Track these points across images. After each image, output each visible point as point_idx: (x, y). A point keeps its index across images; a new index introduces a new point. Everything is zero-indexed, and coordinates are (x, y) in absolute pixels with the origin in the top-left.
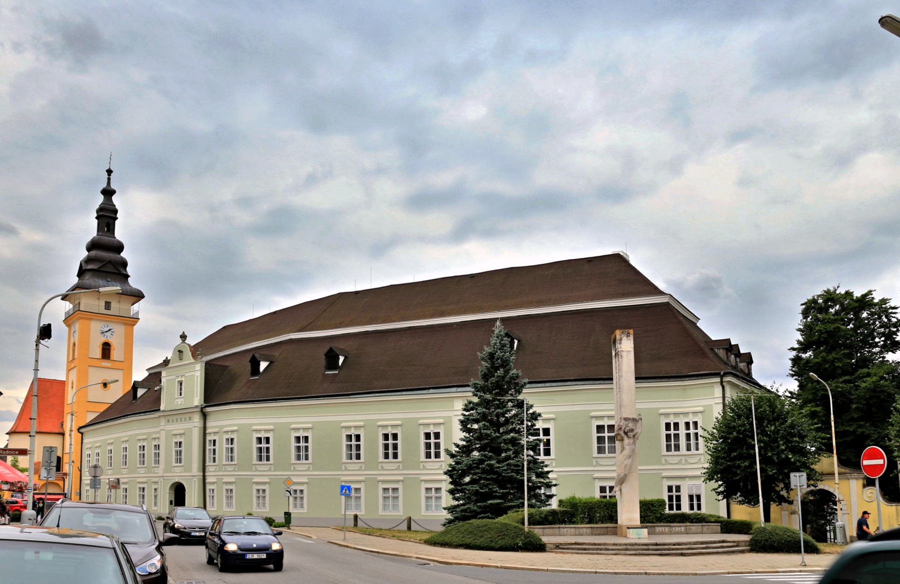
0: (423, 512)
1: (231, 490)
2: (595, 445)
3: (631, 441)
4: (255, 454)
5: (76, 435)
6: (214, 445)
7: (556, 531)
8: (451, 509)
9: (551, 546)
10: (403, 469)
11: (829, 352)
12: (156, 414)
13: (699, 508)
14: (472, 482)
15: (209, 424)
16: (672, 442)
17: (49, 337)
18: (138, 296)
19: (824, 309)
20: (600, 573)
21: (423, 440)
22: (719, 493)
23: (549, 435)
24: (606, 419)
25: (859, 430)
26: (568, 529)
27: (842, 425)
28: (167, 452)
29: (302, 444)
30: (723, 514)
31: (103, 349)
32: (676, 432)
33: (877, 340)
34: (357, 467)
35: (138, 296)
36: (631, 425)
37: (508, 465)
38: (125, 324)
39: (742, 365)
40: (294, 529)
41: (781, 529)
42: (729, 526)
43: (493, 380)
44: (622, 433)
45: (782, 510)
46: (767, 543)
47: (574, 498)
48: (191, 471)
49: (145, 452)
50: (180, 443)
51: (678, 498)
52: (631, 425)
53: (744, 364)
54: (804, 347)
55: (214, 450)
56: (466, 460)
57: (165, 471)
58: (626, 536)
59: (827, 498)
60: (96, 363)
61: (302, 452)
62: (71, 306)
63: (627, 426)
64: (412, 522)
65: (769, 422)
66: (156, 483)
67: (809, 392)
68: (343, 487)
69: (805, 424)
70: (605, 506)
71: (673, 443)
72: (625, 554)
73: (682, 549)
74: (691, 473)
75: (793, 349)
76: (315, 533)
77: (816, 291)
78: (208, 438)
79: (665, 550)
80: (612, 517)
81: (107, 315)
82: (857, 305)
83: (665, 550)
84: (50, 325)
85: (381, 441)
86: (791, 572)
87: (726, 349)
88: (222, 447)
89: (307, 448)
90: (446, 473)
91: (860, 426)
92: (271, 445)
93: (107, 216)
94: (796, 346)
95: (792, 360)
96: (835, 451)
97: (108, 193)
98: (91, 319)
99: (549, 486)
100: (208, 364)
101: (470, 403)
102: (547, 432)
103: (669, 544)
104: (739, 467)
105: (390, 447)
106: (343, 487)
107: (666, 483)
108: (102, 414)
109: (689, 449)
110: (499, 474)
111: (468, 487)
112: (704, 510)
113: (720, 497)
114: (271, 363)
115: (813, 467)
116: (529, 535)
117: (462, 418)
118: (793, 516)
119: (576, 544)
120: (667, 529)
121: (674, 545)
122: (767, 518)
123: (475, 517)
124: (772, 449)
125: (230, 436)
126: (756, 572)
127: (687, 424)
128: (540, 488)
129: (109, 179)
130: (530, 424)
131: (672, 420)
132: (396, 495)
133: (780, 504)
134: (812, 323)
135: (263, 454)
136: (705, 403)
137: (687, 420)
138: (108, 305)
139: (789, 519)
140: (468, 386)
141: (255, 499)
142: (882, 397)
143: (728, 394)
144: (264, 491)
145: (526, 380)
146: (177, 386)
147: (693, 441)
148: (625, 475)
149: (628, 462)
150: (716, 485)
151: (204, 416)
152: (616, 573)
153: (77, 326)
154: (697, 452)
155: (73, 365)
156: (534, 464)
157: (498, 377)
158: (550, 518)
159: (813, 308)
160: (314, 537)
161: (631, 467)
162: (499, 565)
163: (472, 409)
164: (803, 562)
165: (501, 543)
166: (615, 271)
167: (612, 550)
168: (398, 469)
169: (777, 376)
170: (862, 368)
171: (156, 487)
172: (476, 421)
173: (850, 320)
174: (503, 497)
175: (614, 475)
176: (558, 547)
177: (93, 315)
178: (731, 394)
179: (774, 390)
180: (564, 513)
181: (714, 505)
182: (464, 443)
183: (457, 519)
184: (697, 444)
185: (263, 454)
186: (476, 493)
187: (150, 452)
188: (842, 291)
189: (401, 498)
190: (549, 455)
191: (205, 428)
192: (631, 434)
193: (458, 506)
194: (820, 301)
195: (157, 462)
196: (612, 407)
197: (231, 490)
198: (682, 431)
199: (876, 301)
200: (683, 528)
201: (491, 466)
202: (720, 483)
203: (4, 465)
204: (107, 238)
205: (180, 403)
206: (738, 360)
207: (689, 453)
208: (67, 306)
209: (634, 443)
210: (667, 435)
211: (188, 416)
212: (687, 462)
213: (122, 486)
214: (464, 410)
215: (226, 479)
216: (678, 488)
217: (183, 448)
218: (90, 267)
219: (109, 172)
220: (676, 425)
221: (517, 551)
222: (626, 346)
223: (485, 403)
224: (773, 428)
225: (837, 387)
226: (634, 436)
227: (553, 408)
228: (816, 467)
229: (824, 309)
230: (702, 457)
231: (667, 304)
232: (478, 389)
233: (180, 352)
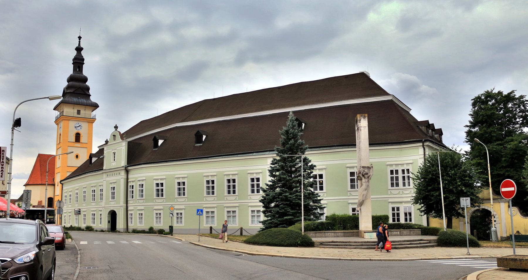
0: (250, 224)
1: (142, 214)
2: (349, 184)
4: (155, 193)
5: (60, 185)
6: (133, 188)
7: (323, 234)
8: (264, 222)
9: (318, 244)
11: (489, 127)
13: (411, 220)
14: (276, 206)
15: (130, 176)
16: (394, 183)
17: (20, 125)
18: (95, 106)
19: (485, 102)
20: (342, 260)
21: (250, 183)
22: (422, 212)
23: (322, 178)
25: (507, 173)
26: (331, 233)
27: (497, 170)
28: (107, 193)
29: (182, 187)
30: (425, 224)
32: (397, 175)
33: (518, 120)
34: (212, 199)
35: (95, 106)
36: (366, 171)
37: (296, 196)
38: (88, 122)
40: (176, 236)
41: (456, 232)
42: (426, 231)
43: (288, 146)
44: (361, 175)
45: (460, 221)
46: (456, 241)
47: (334, 215)
49: (95, 193)
50: (114, 188)
51: (398, 215)
52: (366, 171)
53: (438, 135)
54: (473, 125)
55: (133, 191)
56: (272, 194)
57: (106, 204)
58: (363, 237)
59: (487, 214)
61: (181, 191)
62: (59, 113)
63: (364, 171)
64: (213, 230)
65: (451, 168)
67: (476, 152)
68: (198, 210)
69: (474, 171)
70: (353, 219)
74: (405, 200)
75: (467, 126)
76: (184, 238)
77: (480, 91)
78: (130, 184)
80: (357, 227)
82: (505, 99)
84: (20, 119)
85: (226, 184)
86: (460, 258)
87: (426, 126)
88: (136, 189)
89: (184, 188)
90: (260, 201)
91: (507, 171)
92: (164, 188)
93: (78, 62)
94: (469, 124)
95: (466, 132)
96: (490, 186)
97: (79, 49)
98: (69, 120)
99: (322, 208)
100: (129, 143)
101: (275, 160)
102: (321, 176)
104: (433, 196)
105: (231, 186)
106: (198, 210)
107: (391, 206)
108: (73, 173)
109: (404, 185)
110: (291, 201)
111: (273, 209)
112: (413, 222)
113: (423, 214)
114: (165, 140)
115: (477, 195)
116: (304, 237)
117: (270, 169)
119: (332, 242)
122: (449, 225)
123: (276, 227)
124: (453, 185)
125: (141, 183)
126: (439, 259)
127: (403, 171)
128: (316, 209)
129: (80, 42)
130: (309, 171)
131: (394, 168)
132: (234, 215)
133: (458, 218)
134: (477, 110)
135: (160, 193)
136: (413, 158)
138: (79, 112)
139: (463, 226)
140: (274, 151)
141: (155, 219)
142: (521, 153)
143: (427, 153)
144: (181, 214)
145: (307, 146)
146: (112, 155)
147: (406, 181)
148: (363, 201)
149: (365, 192)
150: (420, 207)
151: (127, 172)
152: (352, 260)
153: (62, 124)
154: (409, 187)
155: (59, 146)
156: (311, 196)
157: (291, 144)
158: (320, 227)
159: (479, 102)
160: (183, 240)
162: (282, 255)
163: (276, 163)
164: (468, 252)
165: (288, 242)
166: (361, 83)
167: (354, 245)
168: (236, 199)
169: (457, 142)
170: (509, 136)
172: (278, 170)
173: (501, 108)
174: (292, 215)
175: (357, 201)
176: (322, 244)
177: (69, 118)
178: (428, 152)
179: (454, 149)
180: (327, 224)
181: (419, 219)
182: (271, 183)
183: (267, 228)
184: (409, 182)
185: (160, 193)
186: (278, 212)
187: (98, 193)
188: (496, 91)
189: (237, 217)
191: (127, 179)
192: (366, 176)
193: (268, 220)
194: (483, 98)
195: (101, 199)
196: (356, 161)
197: (142, 214)
198: (400, 175)
199: (517, 97)
201: (286, 196)
202: (422, 205)
203: (2, 201)
205: (114, 165)
206: (434, 132)
207: (405, 188)
208: (57, 113)
209: (368, 181)
211: (118, 172)
212: (403, 193)
213: (82, 213)
214: (272, 164)
215: (139, 208)
216: (398, 209)
217: (115, 191)
218: (68, 91)
219: (80, 38)
220: (397, 171)
221: (297, 246)
222: (363, 124)
223: (284, 160)
224: (453, 172)
225: (493, 148)
226: (368, 177)
227: (321, 161)
228: (480, 195)
229: (485, 102)
230: (412, 190)
232: (280, 152)
233: (114, 136)
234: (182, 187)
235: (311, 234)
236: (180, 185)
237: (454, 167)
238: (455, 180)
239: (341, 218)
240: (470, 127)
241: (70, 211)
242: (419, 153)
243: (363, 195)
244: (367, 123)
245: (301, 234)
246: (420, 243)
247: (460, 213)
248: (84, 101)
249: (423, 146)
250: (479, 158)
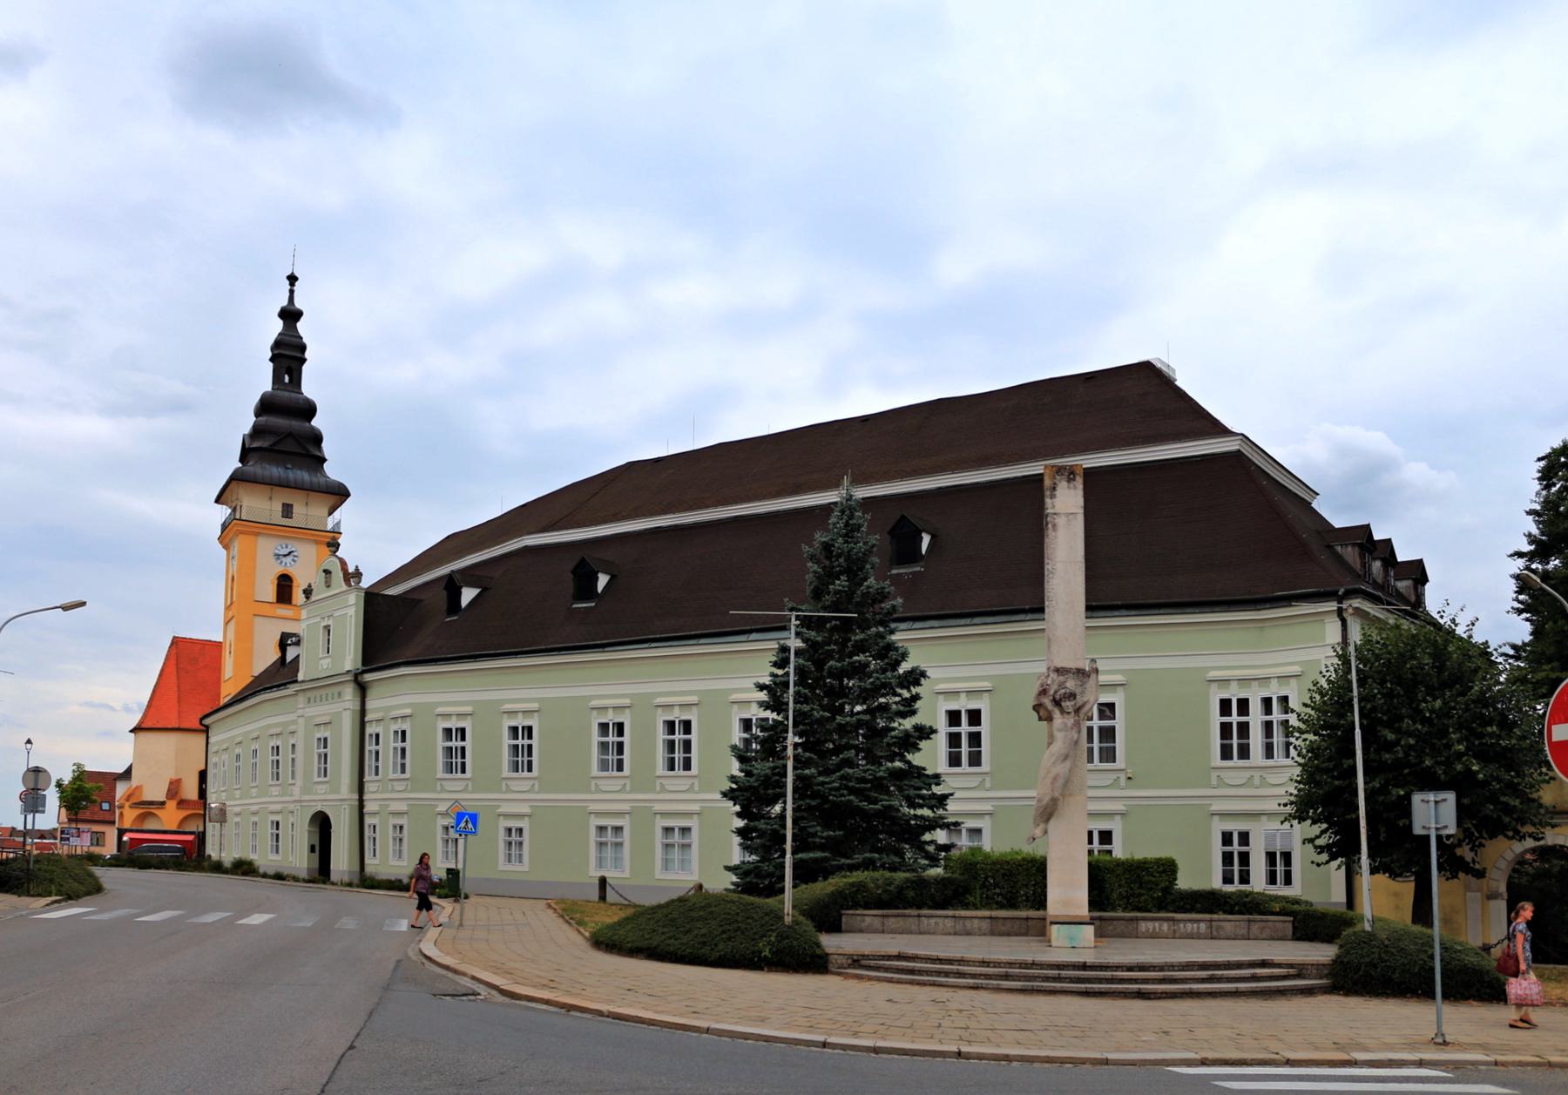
3: (1070, 720)
10: (700, 791)
12: (293, 688)
15: (370, 705)
23: (978, 723)
24: (1234, 684)
28: (306, 757)
29: (678, 737)
31: (279, 586)
35: (339, 494)
37: (843, 778)
38: (317, 542)
39: (1403, 585)
44: (1047, 701)
45: (1467, 888)
48: (338, 791)
51: (1245, 858)
52: (1071, 684)
54: (1541, 550)
57: (304, 790)
60: (267, 609)
61: (522, 758)
64: (608, 889)
65: (1432, 692)
66: (254, 813)
71: (1235, 741)
72: (998, 989)
73: (1145, 981)
75: (1520, 555)
78: (369, 730)
79: (1100, 980)
80: (1039, 900)
81: (284, 528)
83: (1100, 980)
87: (1361, 546)
88: (389, 745)
94: (1527, 548)
97: (290, 315)
98: (257, 534)
103: (1118, 967)
109: (1269, 751)
110: (825, 799)
114: (484, 590)
118: (1493, 903)
119: (899, 957)
120: (1165, 926)
121: (1130, 969)
125: (399, 726)
126: (1289, 1063)
127: (1267, 702)
129: (292, 292)
131: (1234, 693)
132: (686, 841)
136: (1296, 654)
137: (1267, 695)
138: (287, 511)
141: (502, 846)
144: (520, 831)
148: (1054, 801)
150: (1316, 829)
151: (362, 689)
157: (839, 592)
161: (1067, 782)
162: (604, 1008)
165: (723, 948)
167: (973, 976)
168: (690, 790)
171: (255, 819)
177: (260, 528)
179: (1445, 621)
185: (455, 760)
189: (695, 847)
191: (363, 712)
192: (1067, 704)
198: (1256, 718)
200: (1203, 926)
204: (286, 394)
205: (325, 666)
207: (1270, 762)
211: (335, 690)
212: (1264, 783)
215: (395, 806)
216: (1244, 838)
219: (292, 279)
220: (1244, 705)
224: (1438, 703)
226: (1077, 711)
231: (1237, 455)
234: (678, 737)
236: (673, 733)
237: (1445, 685)
238: (1444, 733)
239: (994, 863)
240: (1531, 556)
241: (254, 808)
242: (1324, 639)
243: (1055, 779)
244: (1080, 501)
245: (779, 917)
246: (1254, 978)
247: (1462, 858)
248: (304, 476)
249: (1340, 612)
250: (1555, 664)
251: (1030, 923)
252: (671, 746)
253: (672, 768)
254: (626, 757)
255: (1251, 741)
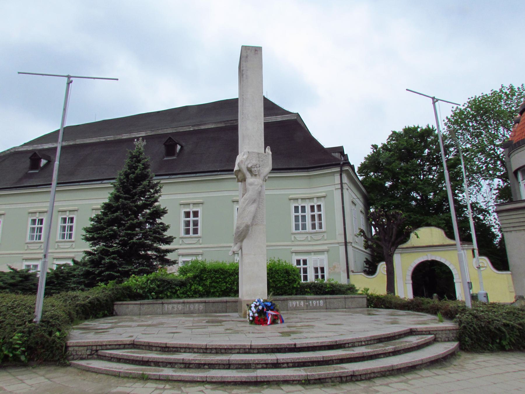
4: (182, 227)
23: (197, 216)
24: (191, 206)
29: (192, 219)
71: (300, 223)
89: (320, 216)
118: (407, 285)
127: (312, 208)
131: (300, 204)
137: (312, 204)
190: (197, 233)
198: (308, 213)
210: (295, 216)
220: (303, 208)
234: (192, 219)
235: (131, 307)
236: (65, 222)
251: (228, 304)
252: (64, 228)
253: (63, 237)
254: (74, 232)
255: (307, 223)
